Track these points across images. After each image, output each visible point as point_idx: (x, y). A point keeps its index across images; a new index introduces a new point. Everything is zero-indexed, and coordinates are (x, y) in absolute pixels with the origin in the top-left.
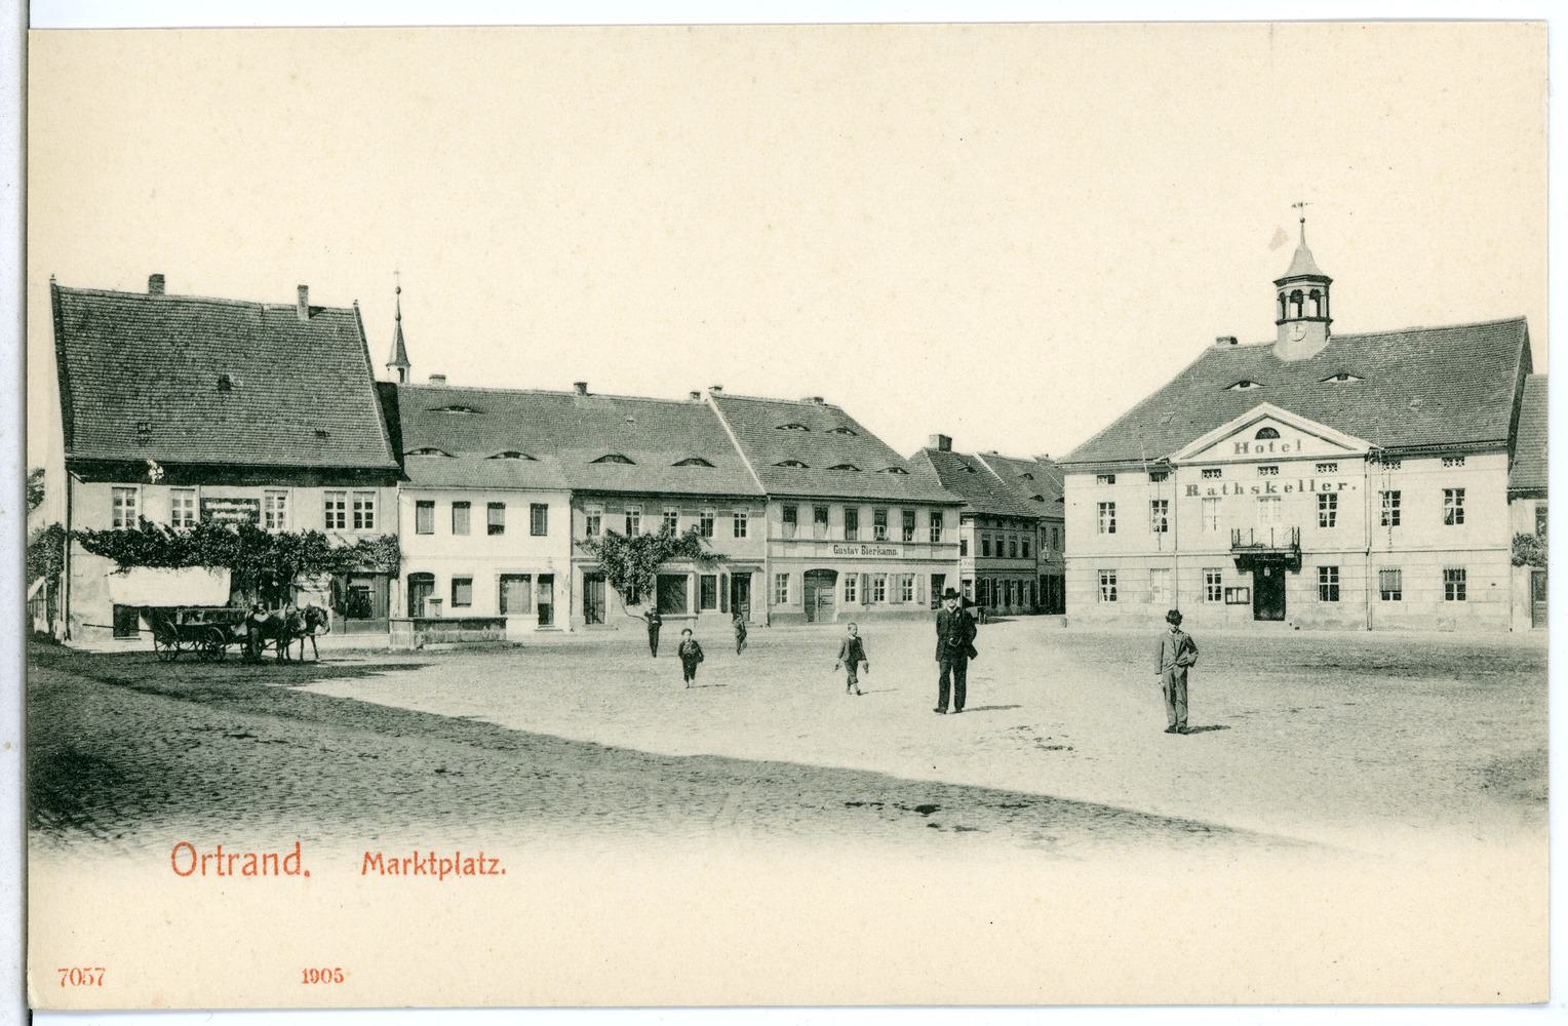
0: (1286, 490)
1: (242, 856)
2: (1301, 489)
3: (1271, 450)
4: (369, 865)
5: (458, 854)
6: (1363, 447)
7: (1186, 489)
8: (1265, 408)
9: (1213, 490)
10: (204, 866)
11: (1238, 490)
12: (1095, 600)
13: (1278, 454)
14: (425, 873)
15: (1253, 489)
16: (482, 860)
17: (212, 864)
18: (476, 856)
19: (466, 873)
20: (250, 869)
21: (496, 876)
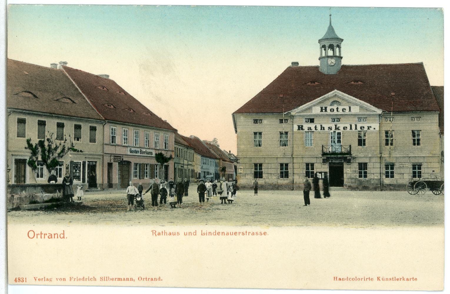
3: (337, 111)
13: (341, 112)
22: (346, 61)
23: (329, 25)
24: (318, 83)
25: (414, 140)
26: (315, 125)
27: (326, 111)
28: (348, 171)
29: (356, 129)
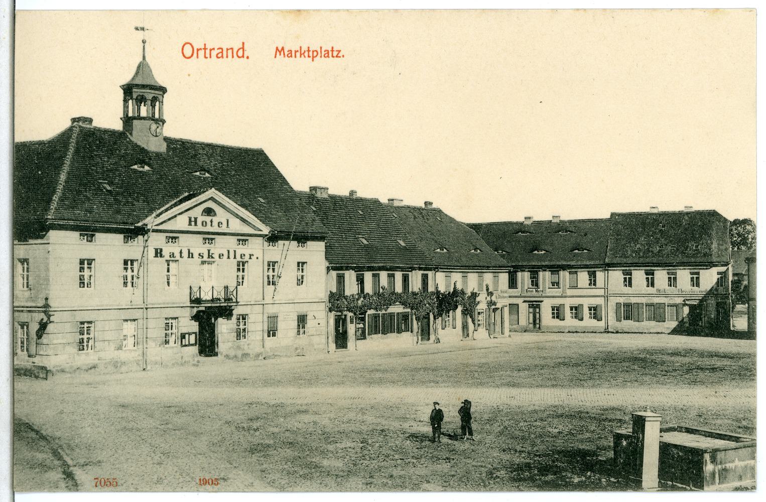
0: (220, 258)
1: (216, 49)
2: (229, 258)
4: (278, 53)
5: (321, 48)
6: (266, 230)
7: (154, 250)
8: (212, 192)
9: (173, 254)
10: (197, 54)
11: (190, 255)
12: (75, 350)
13: (215, 229)
14: (305, 57)
15: (200, 255)
16: (332, 51)
17: (201, 53)
18: (330, 49)
19: (325, 57)
20: (220, 55)
21: (339, 58)
25: (126, 278)
26: (180, 250)
27: (196, 224)
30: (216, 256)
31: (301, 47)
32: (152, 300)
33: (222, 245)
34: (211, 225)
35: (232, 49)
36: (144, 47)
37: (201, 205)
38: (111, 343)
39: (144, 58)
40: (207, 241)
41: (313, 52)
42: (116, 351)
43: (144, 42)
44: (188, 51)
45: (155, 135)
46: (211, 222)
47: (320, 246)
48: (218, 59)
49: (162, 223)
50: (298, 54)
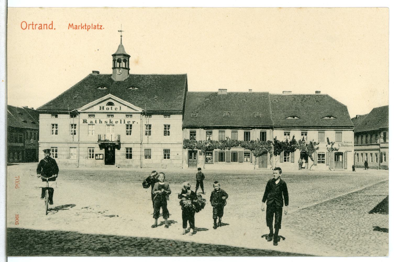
2: (121, 123)
4: (70, 27)
9: (92, 122)
10: (29, 27)
11: (101, 122)
14: (83, 28)
15: (105, 122)
17: (31, 26)
18: (96, 25)
22: (133, 71)
23: (119, 43)
24: (106, 88)
28: (118, 153)
29: (124, 123)
30: (114, 123)
31: (81, 24)
32: (82, 140)
33: (117, 118)
34: (111, 109)
35: (46, 25)
36: (121, 38)
37: (106, 101)
38: (64, 156)
39: (121, 43)
40: (92, 116)
41: (88, 26)
42: (66, 159)
43: (121, 36)
44: (24, 26)
45: (120, 74)
46: (111, 108)
47: (179, 118)
48: (40, 30)
49: (89, 108)
50: (80, 27)
